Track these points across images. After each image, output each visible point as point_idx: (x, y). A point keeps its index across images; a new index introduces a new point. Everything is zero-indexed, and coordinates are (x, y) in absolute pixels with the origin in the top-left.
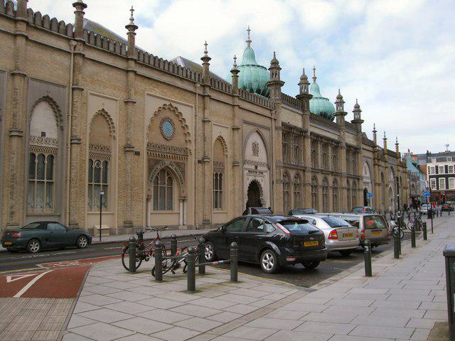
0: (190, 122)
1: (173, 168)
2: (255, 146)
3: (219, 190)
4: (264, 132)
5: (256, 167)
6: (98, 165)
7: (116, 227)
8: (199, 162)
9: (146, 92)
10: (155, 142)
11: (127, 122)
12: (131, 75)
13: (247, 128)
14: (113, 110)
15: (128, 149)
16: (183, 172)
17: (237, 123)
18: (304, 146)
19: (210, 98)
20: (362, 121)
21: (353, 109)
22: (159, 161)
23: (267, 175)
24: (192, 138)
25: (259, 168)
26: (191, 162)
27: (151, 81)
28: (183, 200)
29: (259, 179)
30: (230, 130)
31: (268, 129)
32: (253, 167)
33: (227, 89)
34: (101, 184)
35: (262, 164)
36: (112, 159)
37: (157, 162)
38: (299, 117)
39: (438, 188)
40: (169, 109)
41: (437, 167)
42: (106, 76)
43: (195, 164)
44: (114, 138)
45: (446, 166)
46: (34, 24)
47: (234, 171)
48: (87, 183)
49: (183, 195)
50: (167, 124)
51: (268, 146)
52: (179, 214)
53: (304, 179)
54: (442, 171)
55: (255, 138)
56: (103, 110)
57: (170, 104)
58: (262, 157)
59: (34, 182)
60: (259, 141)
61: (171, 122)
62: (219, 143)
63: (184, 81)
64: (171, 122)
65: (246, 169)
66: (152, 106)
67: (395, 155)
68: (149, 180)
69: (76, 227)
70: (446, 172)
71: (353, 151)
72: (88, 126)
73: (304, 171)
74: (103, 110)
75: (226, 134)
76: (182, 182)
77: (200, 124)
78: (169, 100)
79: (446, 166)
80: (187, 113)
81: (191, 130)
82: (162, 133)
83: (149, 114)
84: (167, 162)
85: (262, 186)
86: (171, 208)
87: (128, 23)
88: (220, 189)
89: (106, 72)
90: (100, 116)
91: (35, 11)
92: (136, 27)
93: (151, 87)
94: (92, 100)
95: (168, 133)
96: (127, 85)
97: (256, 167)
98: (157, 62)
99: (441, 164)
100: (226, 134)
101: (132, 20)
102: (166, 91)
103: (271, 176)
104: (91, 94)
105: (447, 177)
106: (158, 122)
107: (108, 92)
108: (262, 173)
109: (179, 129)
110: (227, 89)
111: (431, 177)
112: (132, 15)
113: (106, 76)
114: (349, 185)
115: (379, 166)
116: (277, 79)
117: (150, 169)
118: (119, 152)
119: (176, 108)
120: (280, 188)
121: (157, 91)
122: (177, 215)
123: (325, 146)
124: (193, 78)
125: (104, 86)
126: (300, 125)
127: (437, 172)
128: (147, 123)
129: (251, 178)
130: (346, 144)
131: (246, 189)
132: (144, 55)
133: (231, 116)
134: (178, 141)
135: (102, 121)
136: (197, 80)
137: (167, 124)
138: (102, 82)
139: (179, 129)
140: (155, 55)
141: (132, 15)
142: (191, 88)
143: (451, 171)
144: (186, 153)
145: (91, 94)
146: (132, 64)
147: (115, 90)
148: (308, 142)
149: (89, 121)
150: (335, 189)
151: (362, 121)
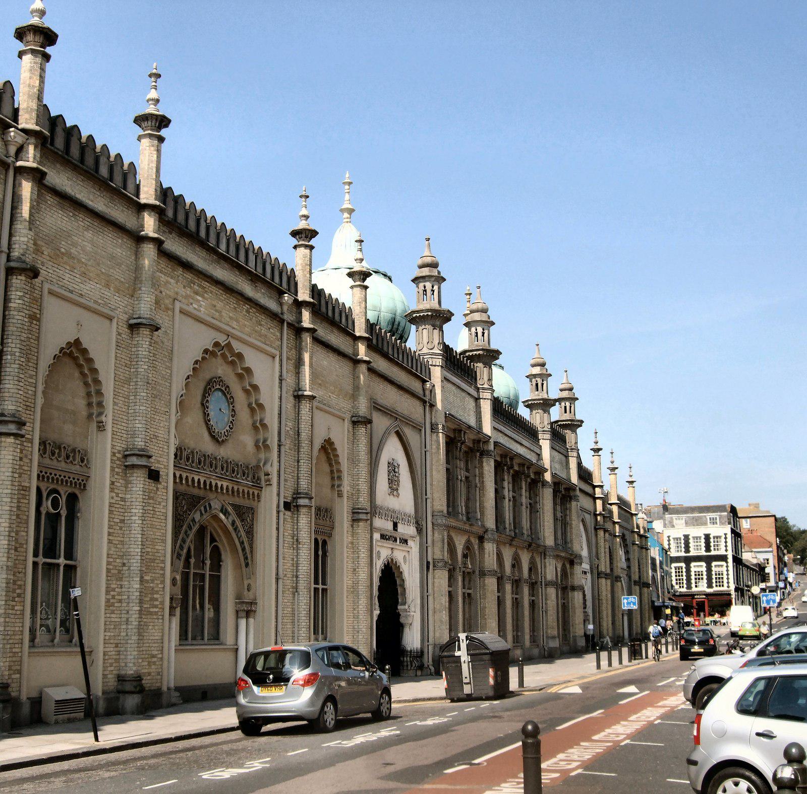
2: (393, 468)
4: (409, 433)
5: (395, 525)
7: (100, 694)
8: (287, 506)
9: (178, 305)
10: (191, 443)
13: (381, 423)
16: (250, 533)
18: (481, 475)
23: (414, 546)
25: (401, 528)
26: (269, 502)
30: (347, 424)
32: (389, 526)
33: (401, 356)
35: (405, 518)
36: (92, 484)
39: (689, 587)
40: (224, 356)
41: (686, 537)
42: (89, 248)
43: (278, 512)
44: (101, 427)
46: (256, 270)
47: (353, 534)
48: (31, 559)
49: (248, 597)
51: (418, 483)
54: (698, 548)
55: (393, 450)
56: (77, 342)
57: (229, 345)
61: (226, 392)
62: (322, 452)
63: (259, 285)
65: (378, 530)
66: (190, 342)
68: (176, 555)
69: (263, 483)
70: (708, 549)
72: (40, 388)
74: (77, 342)
75: (340, 434)
76: (247, 560)
77: (289, 403)
79: (707, 537)
80: (265, 372)
81: (271, 419)
82: (207, 422)
86: (216, 636)
88: (324, 583)
89: (89, 235)
90: (67, 360)
93: (188, 291)
94: (54, 310)
96: (136, 278)
97: (395, 525)
99: (697, 532)
100: (340, 434)
103: (423, 550)
105: (709, 560)
109: (244, 415)
110: (401, 356)
113: (89, 248)
115: (605, 531)
118: (112, 469)
119: (240, 356)
120: (440, 579)
121: (206, 303)
123: (516, 478)
124: (277, 279)
125: (84, 274)
127: (687, 550)
128: (178, 386)
133: (349, 388)
134: (240, 448)
135: (69, 368)
136: (285, 285)
137: (216, 402)
138: (79, 261)
139: (244, 415)
140: (177, 193)
143: (717, 547)
144: (254, 475)
145: (51, 293)
147: (107, 286)
148: (489, 467)
150: (533, 586)
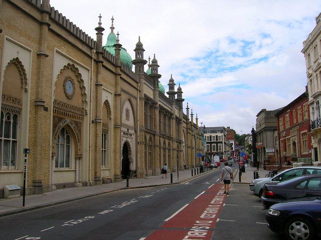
0: (86, 84)
1: (72, 127)
3: (11, 139)
5: (128, 130)
6: (9, 118)
11: (38, 73)
12: (45, 28)
14: (27, 61)
15: (38, 105)
16: (80, 131)
17: (119, 92)
19: (121, 77)
20: (160, 76)
21: (135, 47)
22: (62, 119)
24: (88, 100)
27: (59, 39)
28: (79, 157)
29: (129, 140)
30: (113, 95)
31: (136, 98)
34: (11, 139)
37: (60, 119)
38: (152, 92)
44: (26, 91)
45: (217, 136)
50: (68, 84)
52: (75, 171)
53: (154, 142)
54: (214, 139)
55: (127, 105)
58: (131, 122)
59: (10, 141)
60: (130, 108)
61: (72, 81)
64: (72, 81)
66: (59, 63)
67: (195, 126)
70: (217, 140)
71: (178, 121)
73: (154, 135)
78: (73, 61)
81: (87, 92)
83: (57, 71)
84: (68, 120)
85: (131, 146)
87: (97, 26)
89: (23, 20)
90: (13, 65)
91: (55, 10)
92: (103, 29)
94: (8, 46)
95: (70, 91)
97: (128, 130)
98: (72, 26)
99: (214, 135)
101: (100, 24)
102: (70, 50)
103: (136, 137)
104: (7, 39)
105: (217, 143)
106: (63, 79)
107: (22, 41)
108: (131, 135)
111: (207, 143)
112: (100, 20)
114: (165, 145)
116: (172, 91)
117: (55, 126)
119: (77, 69)
122: (73, 173)
126: (152, 97)
128: (55, 79)
129: (124, 139)
130: (176, 116)
131: (122, 145)
132: (89, 39)
133: (114, 84)
134: (76, 102)
139: (78, 90)
140: (89, 36)
141: (100, 20)
142: (88, 52)
144: (83, 112)
145: (7, 39)
146: (119, 70)
147: (29, 39)
149: (4, 68)
151: (160, 76)
